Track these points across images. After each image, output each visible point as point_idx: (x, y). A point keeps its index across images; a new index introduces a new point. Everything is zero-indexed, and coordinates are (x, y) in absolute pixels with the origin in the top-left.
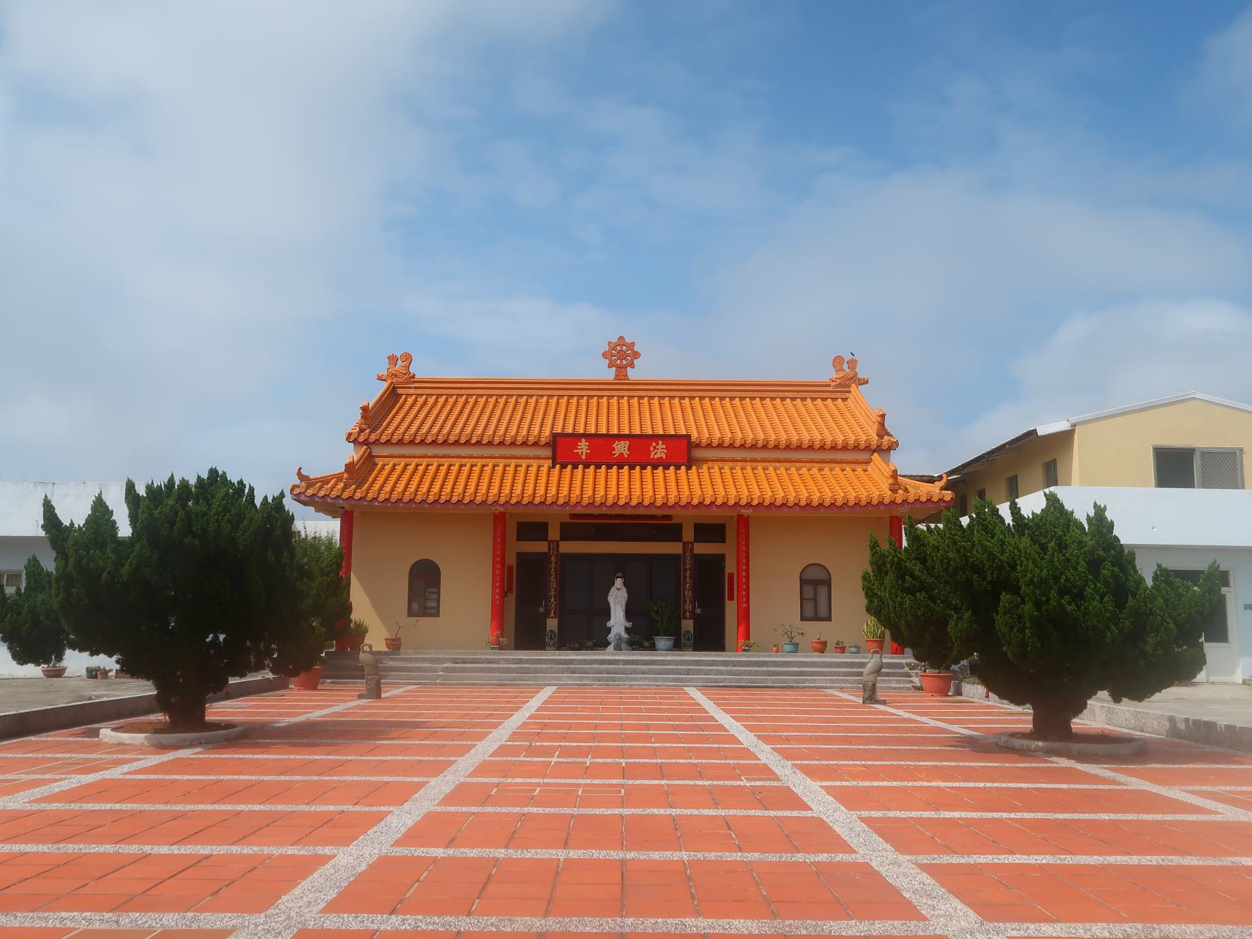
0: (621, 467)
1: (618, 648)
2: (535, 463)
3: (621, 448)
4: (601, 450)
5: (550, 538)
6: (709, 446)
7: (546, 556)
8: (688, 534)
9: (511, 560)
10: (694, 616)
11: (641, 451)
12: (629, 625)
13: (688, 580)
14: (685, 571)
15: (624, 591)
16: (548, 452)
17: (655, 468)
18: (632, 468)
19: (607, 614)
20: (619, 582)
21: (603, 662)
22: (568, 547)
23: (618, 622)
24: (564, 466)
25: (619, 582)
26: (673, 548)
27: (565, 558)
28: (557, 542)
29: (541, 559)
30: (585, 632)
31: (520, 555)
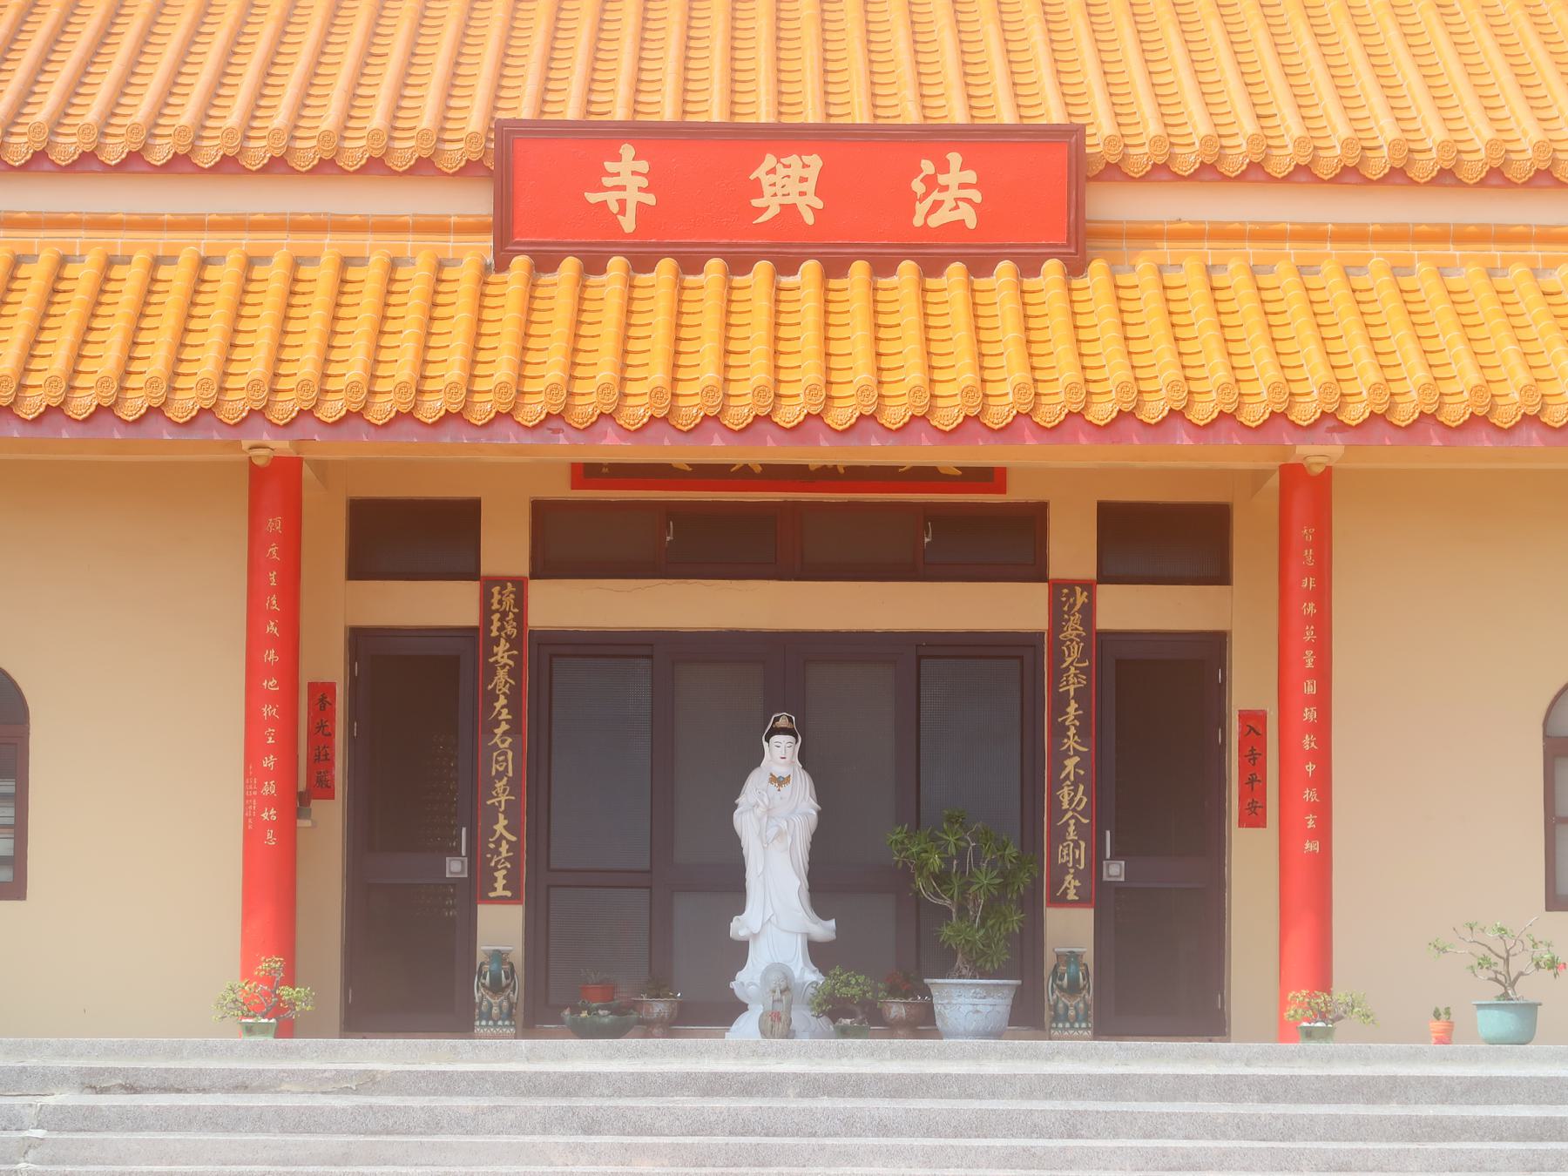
0: (786, 265)
1: (777, 1026)
2: (420, 251)
3: (788, 185)
4: (706, 201)
5: (487, 568)
6: (1161, 173)
7: (473, 639)
8: (1072, 549)
9: (326, 661)
10: (1099, 895)
11: (872, 203)
12: (825, 930)
13: (1072, 742)
16: (477, 203)
17: (932, 266)
18: (834, 268)
19: (727, 880)
20: (780, 752)
21: (715, 1085)
22: (563, 606)
23: (777, 917)
24: (545, 263)
25: (780, 752)
26: (1014, 608)
28: (520, 584)
30: (636, 948)
31: (361, 640)
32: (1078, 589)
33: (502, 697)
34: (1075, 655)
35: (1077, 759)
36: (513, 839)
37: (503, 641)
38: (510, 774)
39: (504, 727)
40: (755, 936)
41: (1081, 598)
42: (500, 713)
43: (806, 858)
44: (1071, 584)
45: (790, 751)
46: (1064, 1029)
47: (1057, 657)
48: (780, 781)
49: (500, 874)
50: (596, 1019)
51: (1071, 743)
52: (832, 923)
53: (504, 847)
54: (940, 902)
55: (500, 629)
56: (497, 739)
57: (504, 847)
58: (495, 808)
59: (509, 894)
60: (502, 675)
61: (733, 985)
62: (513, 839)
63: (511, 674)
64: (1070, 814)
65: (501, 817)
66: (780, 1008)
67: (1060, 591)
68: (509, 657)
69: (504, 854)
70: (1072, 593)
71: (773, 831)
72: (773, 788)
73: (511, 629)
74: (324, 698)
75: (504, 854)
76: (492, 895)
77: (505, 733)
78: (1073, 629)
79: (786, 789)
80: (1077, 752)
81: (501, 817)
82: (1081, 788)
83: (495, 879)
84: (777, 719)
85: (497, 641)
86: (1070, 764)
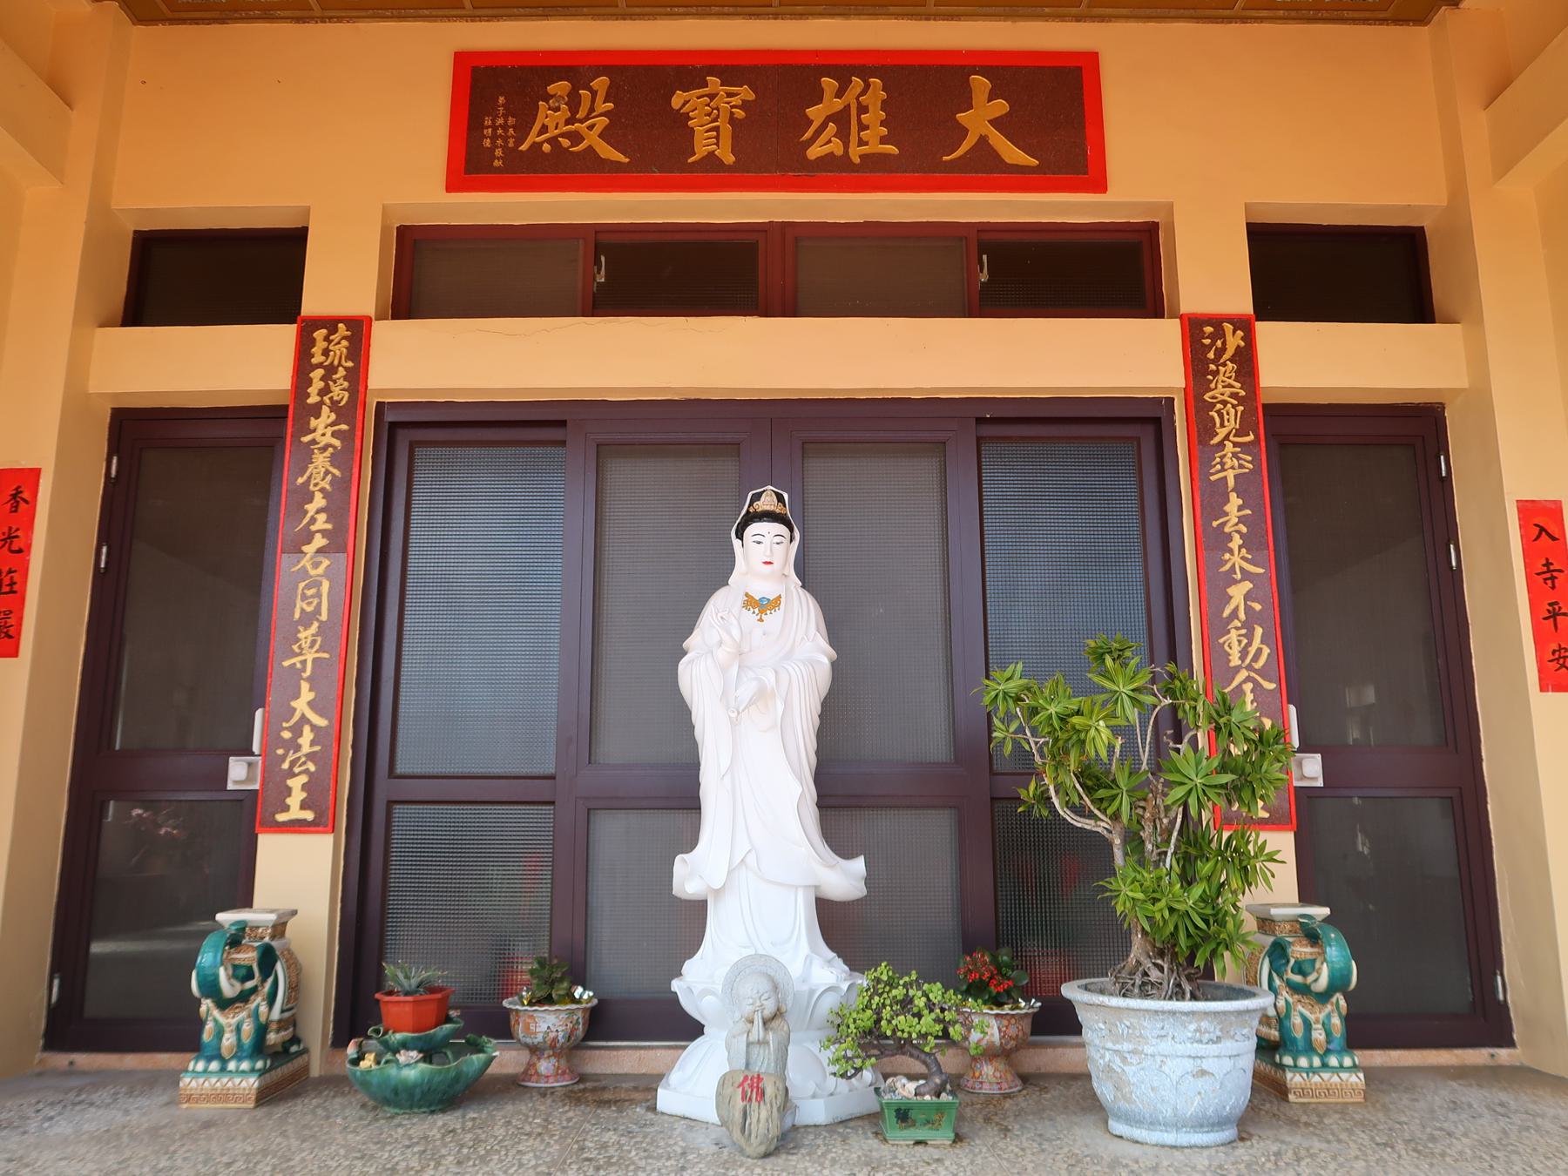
5: (311, 305)
12: (846, 879)
13: (1236, 557)
14: (1210, 502)
15: (802, 619)
20: (763, 556)
22: (427, 360)
25: (763, 556)
26: (1118, 357)
27: (409, 436)
28: (359, 329)
29: (251, 438)
32: (1228, 327)
33: (318, 496)
34: (1232, 424)
35: (1248, 585)
36: (321, 722)
37: (325, 410)
38: (324, 617)
39: (319, 541)
40: (717, 893)
41: (1234, 341)
42: (313, 520)
43: (812, 745)
44: (1217, 321)
45: (780, 550)
46: (1311, 1070)
47: (1202, 429)
48: (761, 606)
49: (296, 783)
50: (392, 1071)
51: (1236, 559)
52: (859, 865)
53: (307, 736)
54: (1087, 824)
55: (324, 391)
56: (306, 562)
57: (307, 736)
58: (295, 673)
59: (309, 815)
60: (321, 461)
61: (676, 985)
62: (321, 722)
63: (334, 460)
64: (1243, 674)
65: (305, 686)
66: (764, 1062)
67: (1200, 336)
68: (334, 434)
69: (306, 749)
70: (1219, 334)
71: (747, 690)
72: (750, 617)
73: (339, 392)
74: (18, 491)
75: (306, 749)
76: (281, 817)
77: (320, 551)
78: (1224, 385)
79: (773, 619)
80: (1246, 575)
81: (305, 686)
82: (1259, 631)
83: (288, 791)
84: (757, 497)
85: (316, 411)
86: (1238, 592)
